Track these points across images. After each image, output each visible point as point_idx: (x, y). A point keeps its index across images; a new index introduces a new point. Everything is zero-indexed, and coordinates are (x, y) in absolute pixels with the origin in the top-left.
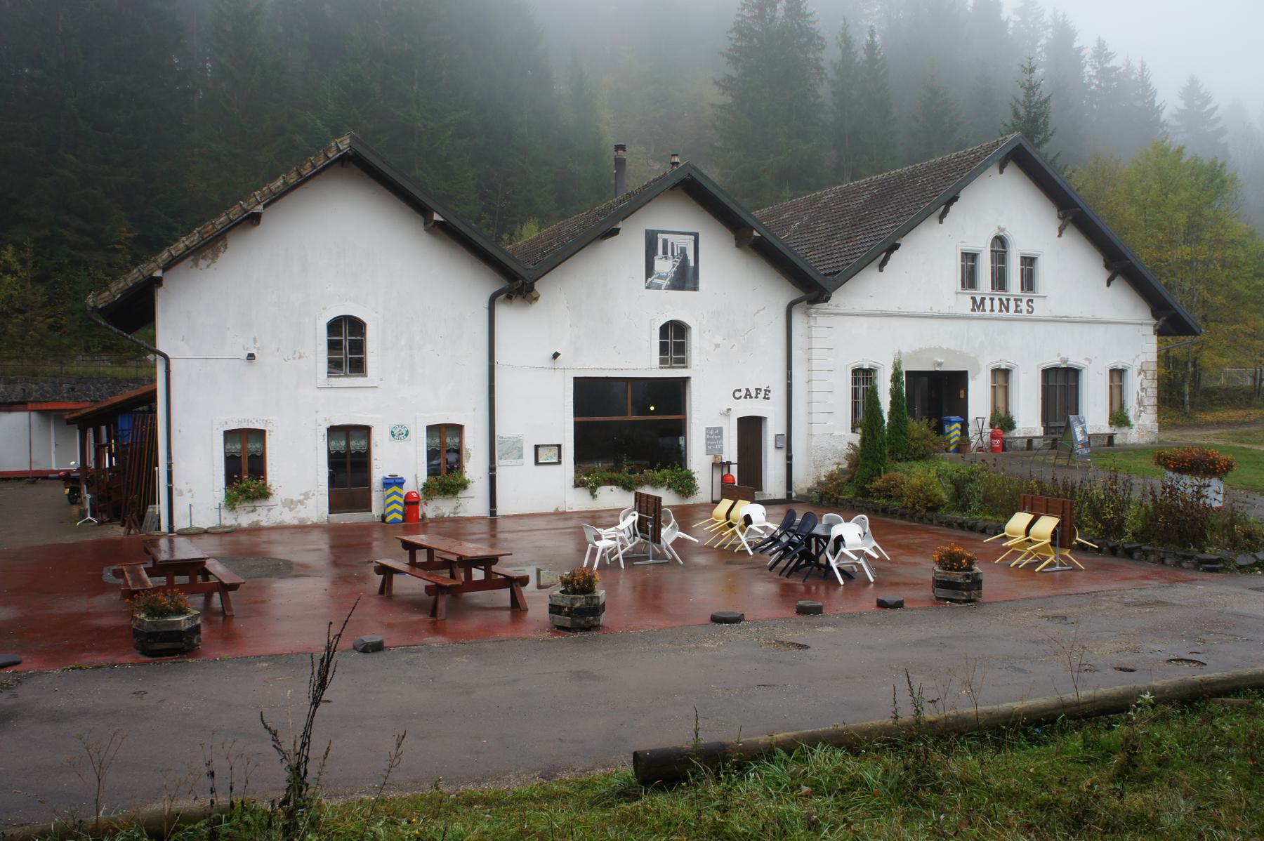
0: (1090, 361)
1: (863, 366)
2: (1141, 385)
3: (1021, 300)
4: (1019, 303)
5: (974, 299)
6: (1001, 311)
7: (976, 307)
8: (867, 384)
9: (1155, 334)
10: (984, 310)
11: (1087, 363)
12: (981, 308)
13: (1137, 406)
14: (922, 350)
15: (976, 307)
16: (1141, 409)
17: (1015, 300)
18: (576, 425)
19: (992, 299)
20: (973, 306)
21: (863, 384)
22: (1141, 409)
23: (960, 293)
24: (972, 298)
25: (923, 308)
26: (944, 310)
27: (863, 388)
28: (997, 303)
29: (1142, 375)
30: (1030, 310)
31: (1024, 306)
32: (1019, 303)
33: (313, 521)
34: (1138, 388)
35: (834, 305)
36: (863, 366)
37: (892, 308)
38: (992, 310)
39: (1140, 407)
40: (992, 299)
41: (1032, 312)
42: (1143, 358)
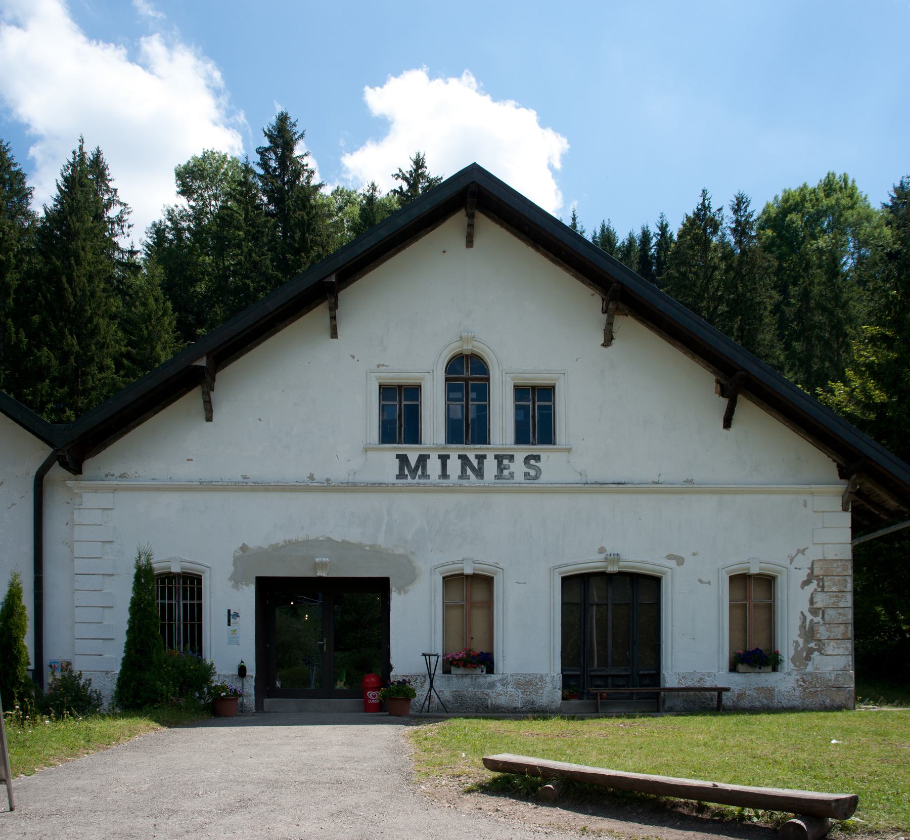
0: (680, 561)
1: (749, 569)
2: (812, 602)
3: (511, 458)
4: (506, 462)
5: (403, 460)
6: (463, 476)
7: (406, 472)
8: (163, 605)
9: (845, 509)
10: (424, 475)
11: (673, 564)
12: (419, 472)
13: (801, 641)
14: (289, 544)
15: (406, 472)
16: (812, 645)
17: (496, 457)
18: (730, 604)
19: (444, 459)
20: (401, 469)
21: (185, 598)
22: (812, 645)
23: (373, 449)
24: (398, 456)
25: (295, 472)
26: (339, 474)
27: (185, 605)
28: (454, 465)
29: (814, 585)
30: (533, 473)
31: (518, 467)
32: (506, 462)
33: (799, 636)
34: (806, 607)
35: (117, 474)
36: (749, 569)
37: (233, 473)
38: (444, 475)
39: (807, 642)
40: (444, 459)
41: (536, 477)
42: (814, 553)
